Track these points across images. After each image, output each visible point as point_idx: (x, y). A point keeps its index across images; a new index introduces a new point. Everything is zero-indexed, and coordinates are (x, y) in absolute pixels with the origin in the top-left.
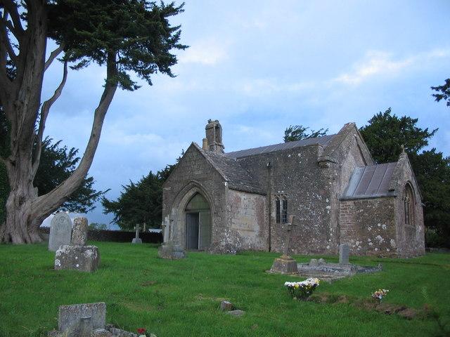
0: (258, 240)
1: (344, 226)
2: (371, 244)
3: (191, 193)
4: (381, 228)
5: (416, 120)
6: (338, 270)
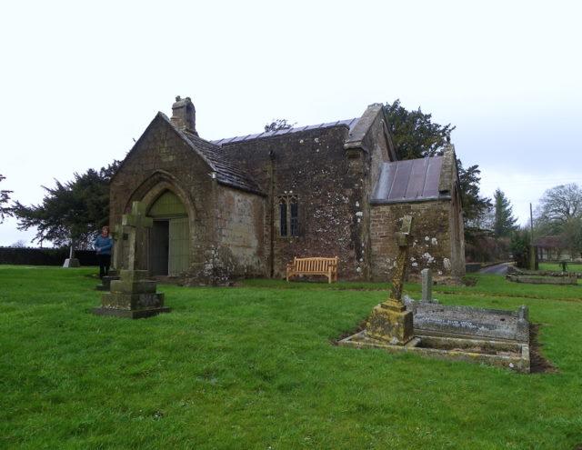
0: (256, 260)
1: (377, 241)
2: (415, 264)
3: (156, 191)
4: (429, 242)
5: (430, 116)
6: (486, 326)
